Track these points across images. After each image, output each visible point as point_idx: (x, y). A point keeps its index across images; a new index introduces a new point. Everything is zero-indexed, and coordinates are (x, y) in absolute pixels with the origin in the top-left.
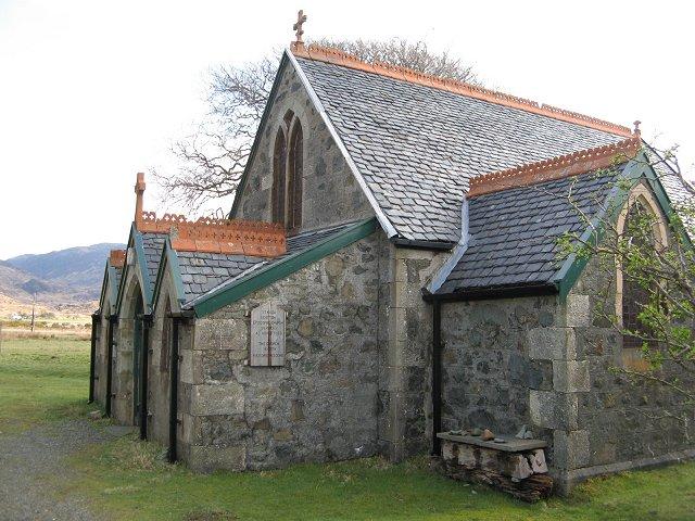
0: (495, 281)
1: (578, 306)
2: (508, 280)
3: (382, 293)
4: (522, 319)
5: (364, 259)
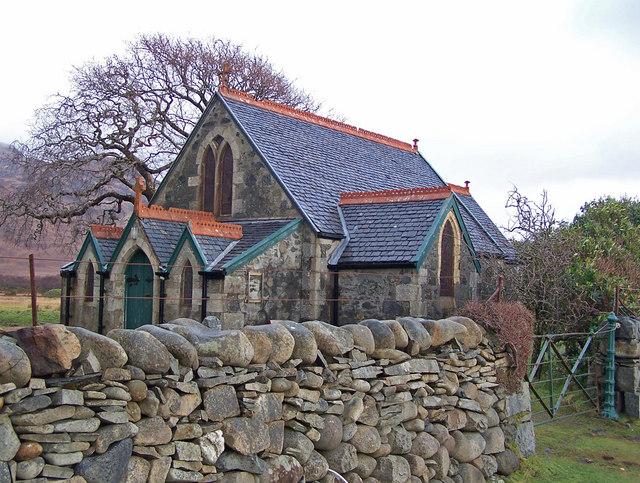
0: (375, 259)
1: (423, 272)
2: (384, 259)
3: (307, 263)
4: (392, 280)
5: (297, 243)
